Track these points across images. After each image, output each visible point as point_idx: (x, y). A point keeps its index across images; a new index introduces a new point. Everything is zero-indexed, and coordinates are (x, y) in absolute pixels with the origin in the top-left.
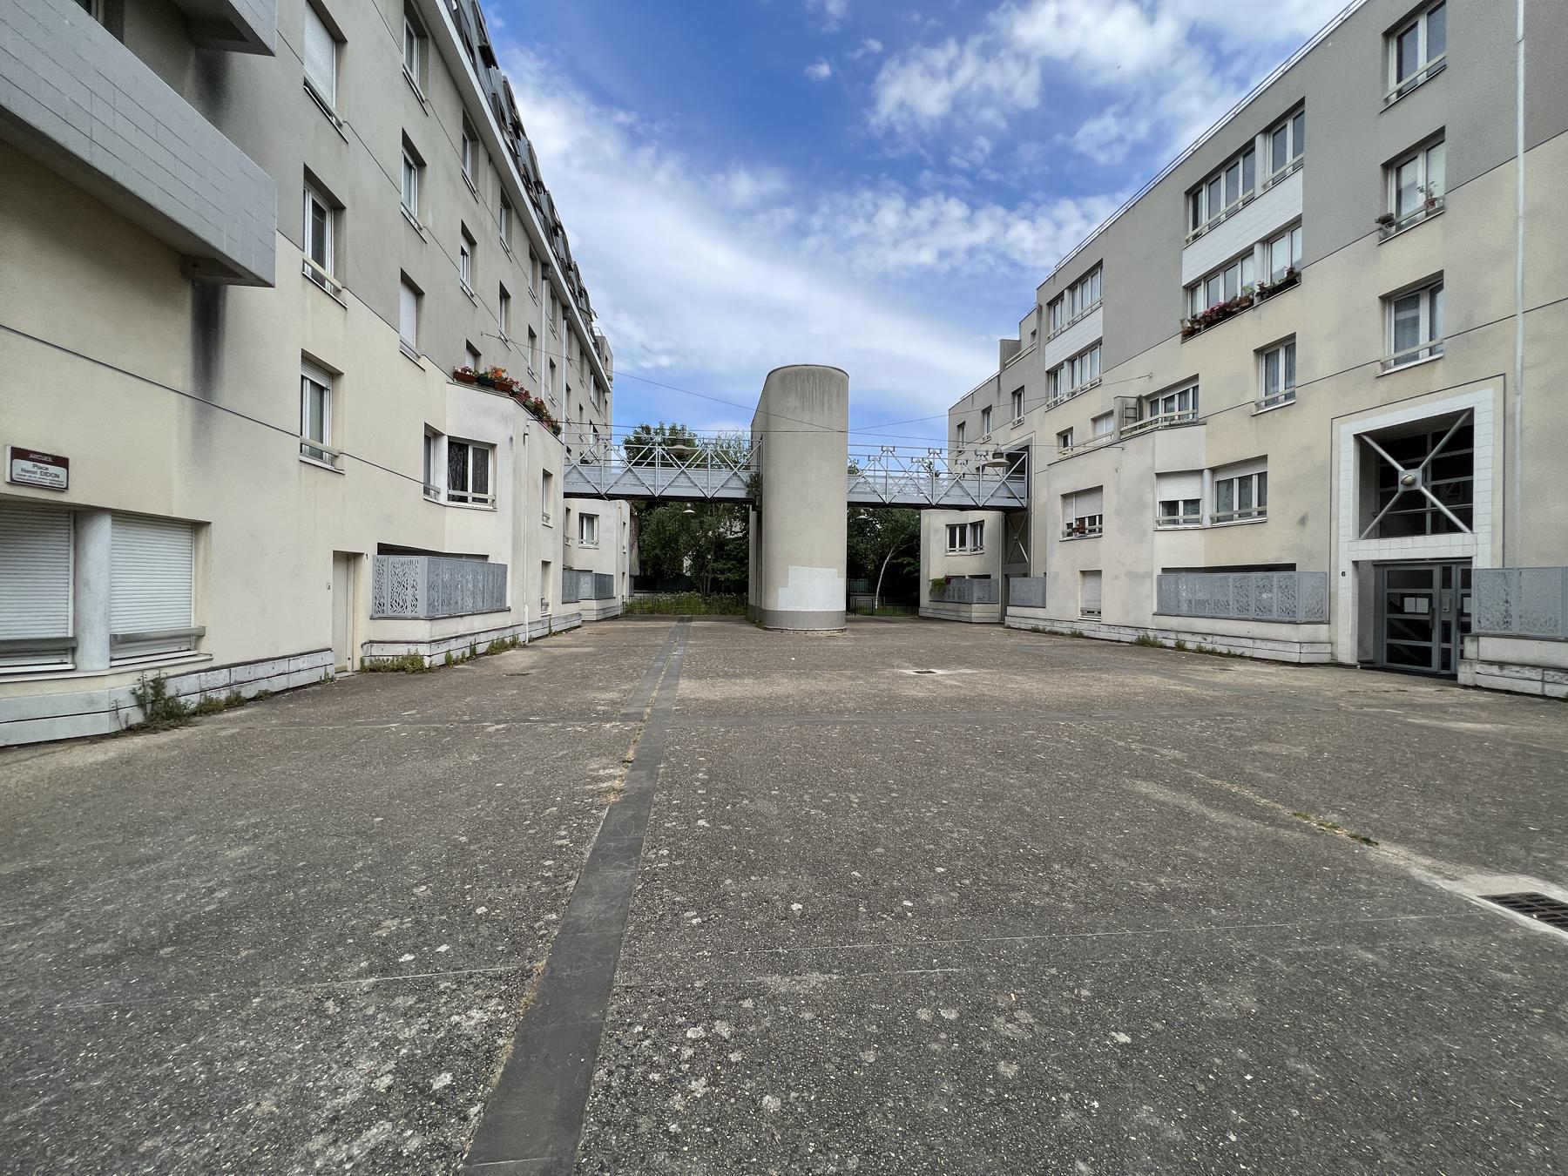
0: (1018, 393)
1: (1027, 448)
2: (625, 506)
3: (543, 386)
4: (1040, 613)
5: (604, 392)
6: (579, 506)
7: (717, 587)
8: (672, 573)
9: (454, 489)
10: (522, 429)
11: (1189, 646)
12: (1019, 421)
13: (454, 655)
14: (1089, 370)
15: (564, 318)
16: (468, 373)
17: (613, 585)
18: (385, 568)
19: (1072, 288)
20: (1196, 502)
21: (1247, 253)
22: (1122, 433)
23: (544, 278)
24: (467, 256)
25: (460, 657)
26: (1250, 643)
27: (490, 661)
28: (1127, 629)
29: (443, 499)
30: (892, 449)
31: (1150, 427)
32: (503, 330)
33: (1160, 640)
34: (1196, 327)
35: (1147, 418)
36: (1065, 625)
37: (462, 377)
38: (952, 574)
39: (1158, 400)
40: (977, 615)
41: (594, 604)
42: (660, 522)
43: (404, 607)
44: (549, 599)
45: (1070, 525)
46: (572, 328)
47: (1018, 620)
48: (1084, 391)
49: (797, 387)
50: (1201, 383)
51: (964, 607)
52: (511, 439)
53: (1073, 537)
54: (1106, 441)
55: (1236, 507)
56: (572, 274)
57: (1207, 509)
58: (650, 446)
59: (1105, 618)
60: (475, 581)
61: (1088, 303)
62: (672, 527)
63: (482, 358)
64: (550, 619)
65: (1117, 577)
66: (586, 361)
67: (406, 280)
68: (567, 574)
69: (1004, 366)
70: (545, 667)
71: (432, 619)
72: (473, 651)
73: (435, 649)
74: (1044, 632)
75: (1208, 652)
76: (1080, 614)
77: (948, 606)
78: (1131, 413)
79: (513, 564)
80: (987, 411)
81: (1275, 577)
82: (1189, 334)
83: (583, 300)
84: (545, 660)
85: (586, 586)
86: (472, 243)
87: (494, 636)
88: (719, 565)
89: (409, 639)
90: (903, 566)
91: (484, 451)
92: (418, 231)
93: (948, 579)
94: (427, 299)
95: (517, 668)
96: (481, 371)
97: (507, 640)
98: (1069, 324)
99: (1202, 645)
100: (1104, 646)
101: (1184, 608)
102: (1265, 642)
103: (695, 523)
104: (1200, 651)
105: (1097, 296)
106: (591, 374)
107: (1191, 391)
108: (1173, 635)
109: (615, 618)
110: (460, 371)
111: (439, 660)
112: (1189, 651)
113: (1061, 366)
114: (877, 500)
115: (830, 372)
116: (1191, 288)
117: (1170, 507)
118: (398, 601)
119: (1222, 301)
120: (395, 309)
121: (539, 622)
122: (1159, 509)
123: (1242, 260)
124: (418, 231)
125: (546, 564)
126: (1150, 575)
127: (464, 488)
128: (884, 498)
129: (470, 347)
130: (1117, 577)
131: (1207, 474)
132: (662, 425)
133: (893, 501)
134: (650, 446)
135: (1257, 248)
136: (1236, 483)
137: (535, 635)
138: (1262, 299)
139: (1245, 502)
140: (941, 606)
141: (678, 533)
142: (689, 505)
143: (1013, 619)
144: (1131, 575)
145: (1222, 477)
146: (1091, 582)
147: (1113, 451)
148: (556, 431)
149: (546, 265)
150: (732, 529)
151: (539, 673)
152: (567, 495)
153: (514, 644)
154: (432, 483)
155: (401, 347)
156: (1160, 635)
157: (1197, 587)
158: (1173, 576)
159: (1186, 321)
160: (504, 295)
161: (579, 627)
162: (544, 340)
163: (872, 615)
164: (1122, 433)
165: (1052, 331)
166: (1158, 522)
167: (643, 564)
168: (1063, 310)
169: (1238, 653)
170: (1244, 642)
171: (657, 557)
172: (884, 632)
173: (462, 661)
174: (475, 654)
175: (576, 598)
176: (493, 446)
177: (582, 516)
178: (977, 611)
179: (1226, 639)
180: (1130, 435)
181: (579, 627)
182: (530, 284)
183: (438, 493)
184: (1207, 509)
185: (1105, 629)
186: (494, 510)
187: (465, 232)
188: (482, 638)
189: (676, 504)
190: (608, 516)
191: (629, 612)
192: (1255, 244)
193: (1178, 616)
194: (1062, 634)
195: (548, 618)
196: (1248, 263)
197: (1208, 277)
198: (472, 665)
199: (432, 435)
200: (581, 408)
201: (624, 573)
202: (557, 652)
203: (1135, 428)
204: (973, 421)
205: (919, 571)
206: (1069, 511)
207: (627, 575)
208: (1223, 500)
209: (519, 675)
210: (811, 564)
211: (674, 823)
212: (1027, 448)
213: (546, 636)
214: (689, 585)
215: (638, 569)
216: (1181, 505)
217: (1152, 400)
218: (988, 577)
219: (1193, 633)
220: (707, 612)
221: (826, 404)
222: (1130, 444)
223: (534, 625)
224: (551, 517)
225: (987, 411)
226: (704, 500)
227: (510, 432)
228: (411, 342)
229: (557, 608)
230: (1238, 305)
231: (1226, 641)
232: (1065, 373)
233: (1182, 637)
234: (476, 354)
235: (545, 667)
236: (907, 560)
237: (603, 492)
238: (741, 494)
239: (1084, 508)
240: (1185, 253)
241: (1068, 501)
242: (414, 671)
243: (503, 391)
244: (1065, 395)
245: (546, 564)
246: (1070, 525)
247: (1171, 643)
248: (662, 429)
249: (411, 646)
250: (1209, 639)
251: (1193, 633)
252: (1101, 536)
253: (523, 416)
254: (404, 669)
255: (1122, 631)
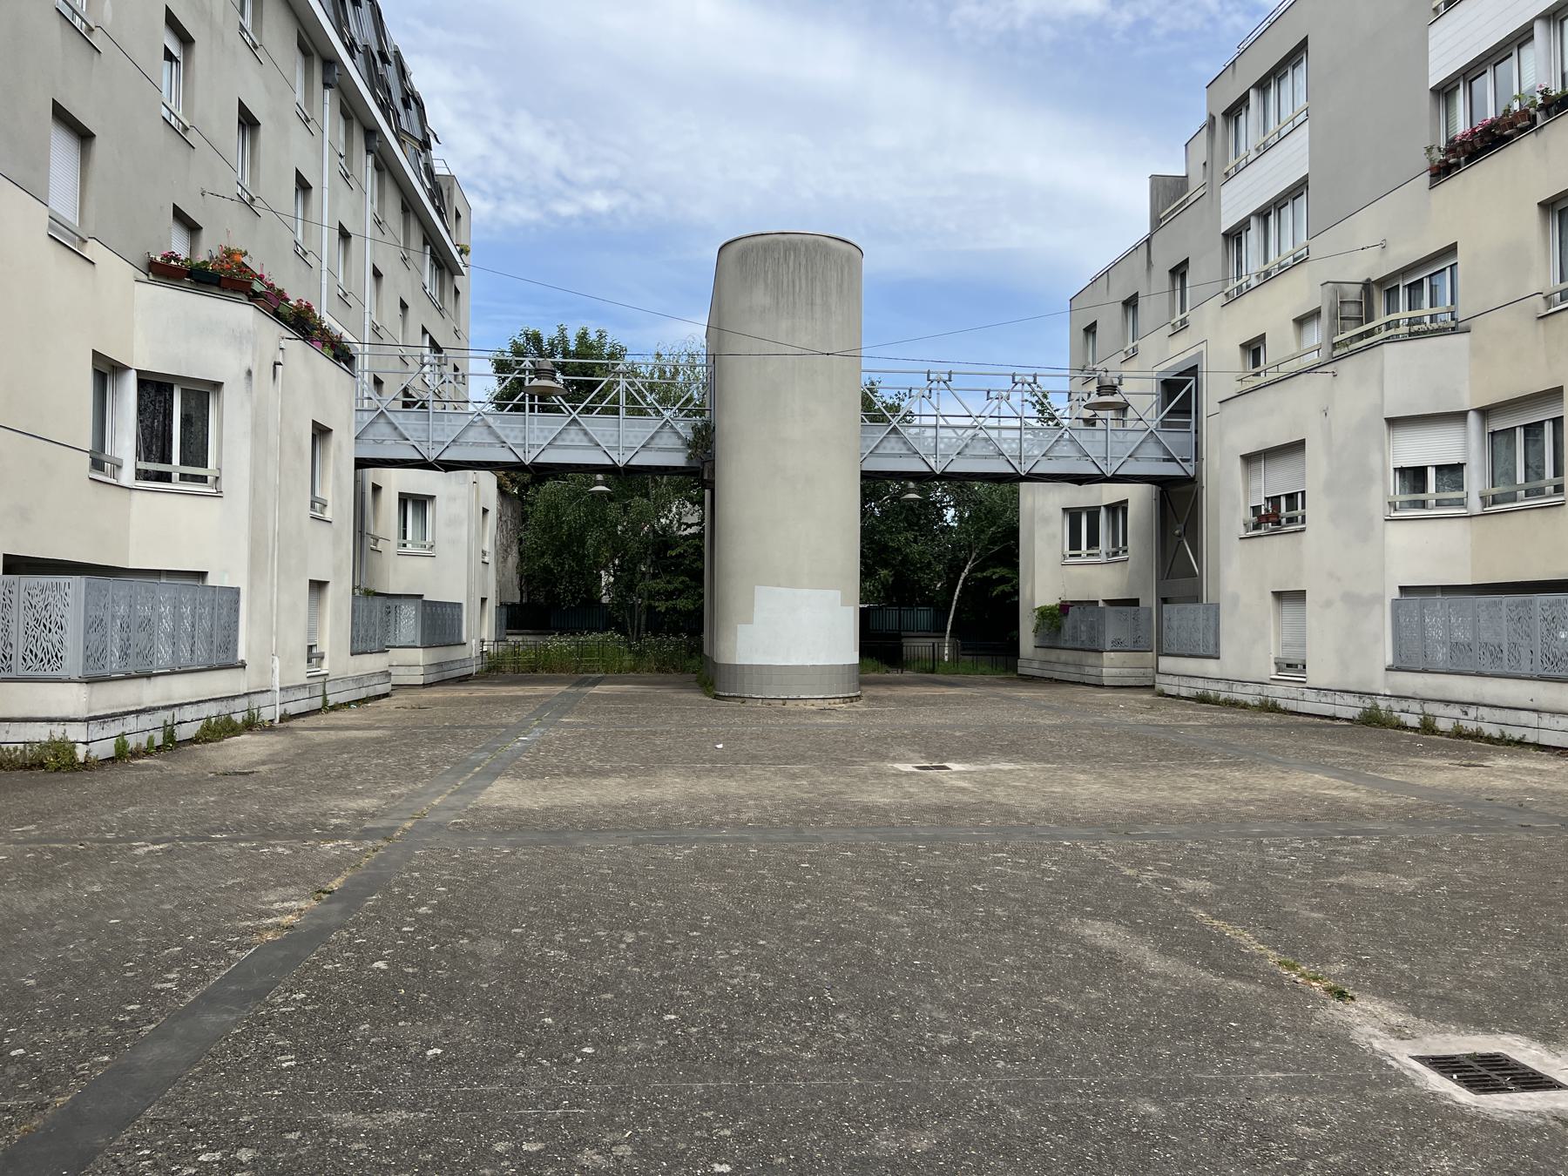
0: (1179, 272)
1: (1193, 371)
2: (488, 480)
3: (325, 274)
4: (1210, 667)
5: (452, 275)
6: (395, 482)
7: (656, 623)
8: (574, 599)
9: (147, 460)
10: (271, 354)
11: (1442, 724)
12: (1183, 321)
13: (133, 741)
14: (1291, 231)
15: (368, 151)
16: (173, 262)
17: (460, 620)
18: (14, 597)
19: (1262, 85)
20: (1458, 468)
21: (1522, 37)
22: (1334, 346)
23: (326, 85)
24: (177, 61)
25: (145, 745)
26: (1531, 718)
27: (198, 753)
28: (1346, 696)
29: (127, 476)
30: (946, 377)
31: (1384, 334)
32: (246, 183)
33: (1395, 714)
34: (1452, 161)
35: (1381, 318)
36: (1251, 689)
37: (164, 271)
38: (1069, 599)
39: (1398, 286)
40: (1114, 671)
41: (419, 656)
42: (553, 507)
43: (45, 661)
44: (324, 646)
45: (1256, 509)
46: (385, 166)
47: (1176, 680)
48: (1284, 269)
49: (766, 273)
50: (1461, 257)
51: (1091, 658)
52: (249, 373)
53: (1262, 532)
54: (1314, 358)
55: (1520, 478)
56: (391, 73)
57: (1475, 482)
58: (516, 375)
59: (1315, 676)
60: (177, 617)
61: (1287, 113)
62: (572, 515)
63: (204, 233)
64: (325, 683)
65: (1328, 604)
66: (414, 225)
67: (61, 115)
68: (362, 603)
69: (1157, 223)
70: (285, 762)
71: (90, 681)
72: (169, 736)
73: (96, 731)
74: (1215, 702)
75: (1470, 736)
76: (1273, 669)
77: (1065, 656)
78: (1352, 310)
79: (251, 586)
80: (1131, 303)
81: (1505, 603)
82: (1441, 172)
83: (413, 113)
84: (292, 751)
85: (408, 622)
86: (186, 40)
87: (211, 710)
88: (660, 585)
89: (53, 715)
90: (989, 583)
91: (202, 394)
92: (84, 36)
93: (1065, 607)
94: (99, 147)
95: (237, 763)
96: (202, 256)
97: (238, 718)
98: (1257, 149)
99: (1461, 723)
100: (1289, 726)
101: (1440, 655)
102: (1557, 718)
103: (613, 510)
104: (1459, 734)
105: (1302, 102)
106: (425, 243)
107: (1448, 270)
108: (1415, 707)
109: (463, 680)
110: (159, 259)
111: (105, 749)
112: (1442, 733)
113: (1244, 225)
114: (917, 466)
115: (826, 245)
116: (1445, 92)
117: (1414, 477)
118: (34, 650)
119: (1491, 115)
120: (41, 166)
121: (304, 686)
122: (1393, 482)
123: (1520, 47)
124: (84, 36)
125: (318, 586)
126: (1379, 599)
127: (166, 458)
128: (933, 465)
129: (179, 215)
130: (1328, 604)
131: (1473, 418)
132: (562, 331)
133: (948, 470)
134: (516, 375)
135: (1539, 28)
136: (1520, 434)
137: (292, 709)
138: (1548, 115)
139: (1534, 470)
140: (1053, 655)
141: (584, 528)
142: (599, 477)
143: (1168, 679)
144: (1351, 600)
145: (1498, 425)
146: (1289, 609)
147: (1319, 380)
148: (342, 355)
149: (330, 63)
150: (682, 517)
151: (271, 771)
152: (361, 464)
153: (250, 725)
154: (108, 451)
155: (50, 226)
156: (1396, 705)
157: (1453, 620)
158: (1416, 599)
159: (1435, 151)
160: (248, 122)
161: (386, 695)
162: (326, 192)
163: (933, 671)
164: (1334, 346)
165: (1232, 162)
166: (1392, 505)
167: (527, 579)
168: (1251, 119)
169: (1517, 737)
170: (1525, 717)
171: (546, 569)
172: (946, 700)
173: (148, 751)
174: (172, 741)
175: (381, 643)
176: (217, 386)
177: (404, 499)
178: (1112, 665)
179: (1497, 712)
180: (1346, 350)
181: (386, 695)
182: (299, 96)
183: (119, 467)
184: (1475, 482)
185: (1311, 695)
186: (218, 495)
187: (172, 22)
188: (188, 713)
189: (581, 477)
190: (452, 499)
191: (493, 669)
192: (1533, 21)
193: (1425, 671)
194: (1245, 706)
195: (322, 679)
196: (1527, 52)
197: (1470, 73)
198: (163, 758)
199: (106, 371)
200: (404, 306)
201: (483, 600)
202: (318, 737)
203: (1360, 336)
204: (1110, 318)
205: (1017, 592)
206: (1254, 485)
207: (492, 604)
208: (1499, 469)
209: (236, 773)
210: (793, 583)
211: (338, 965)
212: (1193, 371)
213: (317, 711)
214: (607, 620)
215: (518, 592)
216: (1431, 474)
217: (1387, 286)
218: (1134, 602)
219: (1448, 702)
220: (633, 669)
221: (818, 301)
222: (1346, 367)
223: (290, 693)
224: (329, 504)
225: (1131, 303)
226: (631, 471)
227: (247, 362)
228: (70, 215)
229: (339, 661)
230: (1512, 125)
231: (1499, 715)
232: (1253, 237)
233: (1431, 708)
234: (192, 228)
235: (285, 762)
236: (1000, 572)
237: (432, 456)
238: (679, 460)
239: (1276, 480)
240: (1433, 30)
241: (1254, 466)
242: (60, 768)
243: (235, 291)
244: (1253, 277)
245: (318, 586)
246: (1256, 509)
247: (1413, 721)
248: (564, 340)
249: (54, 727)
250: (1472, 712)
251: (1448, 702)
252: (1303, 530)
253: (272, 332)
254: (42, 765)
255: (1338, 699)
